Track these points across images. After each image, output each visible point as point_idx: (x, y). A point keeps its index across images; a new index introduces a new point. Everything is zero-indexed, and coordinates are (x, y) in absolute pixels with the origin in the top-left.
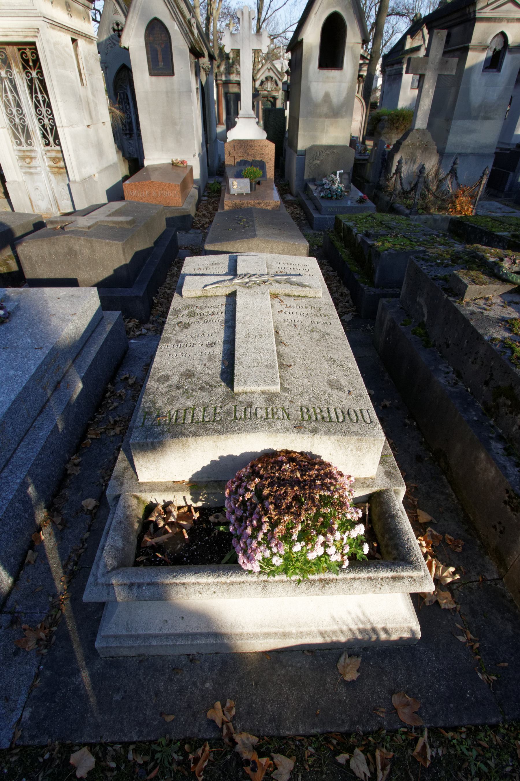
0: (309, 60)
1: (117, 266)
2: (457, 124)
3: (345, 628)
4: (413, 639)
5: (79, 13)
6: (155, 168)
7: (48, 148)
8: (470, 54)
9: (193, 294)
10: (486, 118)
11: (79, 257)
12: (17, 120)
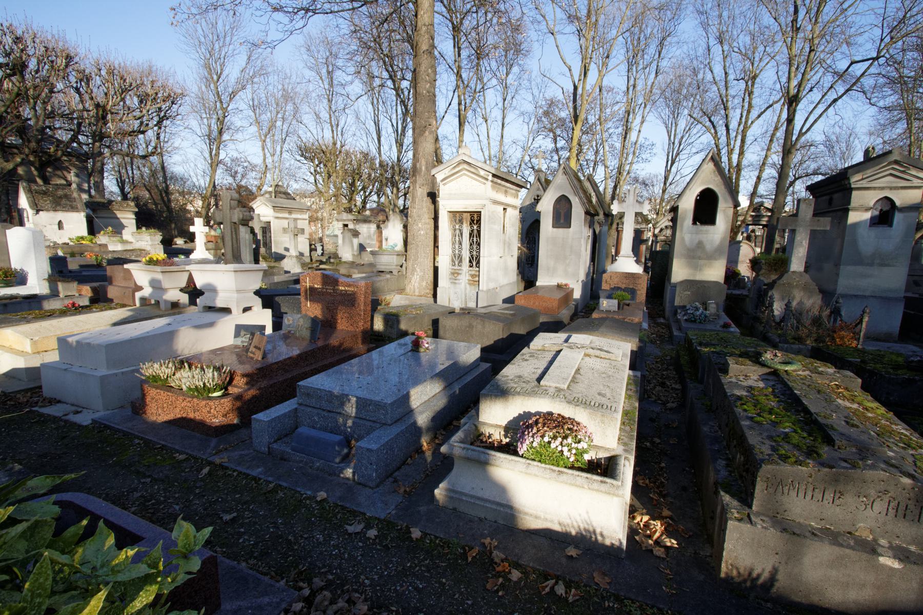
0: (684, 219)
1: (496, 338)
2: (845, 270)
3: (575, 524)
4: (619, 548)
5: (512, 195)
6: (543, 287)
10: (883, 265)
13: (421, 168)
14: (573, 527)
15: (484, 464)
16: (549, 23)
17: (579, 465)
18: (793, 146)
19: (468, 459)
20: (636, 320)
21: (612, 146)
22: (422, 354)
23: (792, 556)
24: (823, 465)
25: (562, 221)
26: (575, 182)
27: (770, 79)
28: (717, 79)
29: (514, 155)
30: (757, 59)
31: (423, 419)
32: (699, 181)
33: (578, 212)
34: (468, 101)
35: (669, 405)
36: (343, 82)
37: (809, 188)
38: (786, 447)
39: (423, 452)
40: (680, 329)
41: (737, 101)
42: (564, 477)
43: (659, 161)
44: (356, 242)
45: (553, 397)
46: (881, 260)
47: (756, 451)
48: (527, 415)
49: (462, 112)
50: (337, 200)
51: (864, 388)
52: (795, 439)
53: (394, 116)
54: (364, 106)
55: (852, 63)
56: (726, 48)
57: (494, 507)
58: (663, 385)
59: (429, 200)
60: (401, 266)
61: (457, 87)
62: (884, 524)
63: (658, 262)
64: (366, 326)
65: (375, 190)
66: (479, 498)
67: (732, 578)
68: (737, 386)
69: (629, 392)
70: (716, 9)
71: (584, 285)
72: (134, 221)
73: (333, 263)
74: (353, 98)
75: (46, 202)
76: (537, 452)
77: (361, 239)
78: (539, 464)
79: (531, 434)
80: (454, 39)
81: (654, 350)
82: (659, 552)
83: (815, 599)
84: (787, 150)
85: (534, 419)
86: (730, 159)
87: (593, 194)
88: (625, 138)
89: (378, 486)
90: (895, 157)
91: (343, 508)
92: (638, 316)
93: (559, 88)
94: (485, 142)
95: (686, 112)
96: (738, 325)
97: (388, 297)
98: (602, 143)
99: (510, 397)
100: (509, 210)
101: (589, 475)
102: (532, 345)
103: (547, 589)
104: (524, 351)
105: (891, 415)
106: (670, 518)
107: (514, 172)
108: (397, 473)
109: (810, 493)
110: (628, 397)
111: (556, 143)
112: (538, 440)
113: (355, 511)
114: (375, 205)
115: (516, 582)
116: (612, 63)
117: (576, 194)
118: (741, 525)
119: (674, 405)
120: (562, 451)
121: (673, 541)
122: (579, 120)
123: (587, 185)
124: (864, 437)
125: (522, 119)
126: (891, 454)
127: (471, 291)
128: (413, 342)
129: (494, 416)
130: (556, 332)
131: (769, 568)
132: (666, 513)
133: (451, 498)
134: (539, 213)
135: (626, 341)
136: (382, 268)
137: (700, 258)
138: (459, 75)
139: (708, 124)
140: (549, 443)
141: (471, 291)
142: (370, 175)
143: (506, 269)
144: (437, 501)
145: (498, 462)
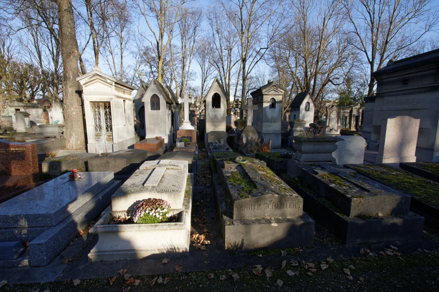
0: (208, 106)
1: (123, 167)
2: (265, 124)
4: (186, 252)
5: (128, 93)
8: (264, 104)
9: (143, 169)
10: (274, 122)
11: (110, 164)
12: (98, 123)
13: (69, 77)
14: (165, 249)
15: (117, 232)
16: (142, 9)
17: (165, 220)
18: (246, 77)
19: (106, 232)
20: (193, 150)
21: (178, 73)
22: (76, 182)
23: (247, 233)
24: (253, 196)
25: (155, 107)
26: (160, 88)
27: (236, 51)
28: (218, 48)
29: (130, 73)
30: (231, 42)
31: (78, 218)
32: (213, 90)
33: (163, 102)
34: (99, 42)
35: (207, 185)
36: (6, 18)
37: (251, 94)
38: (243, 192)
39: (81, 236)
40: (211, 152)
41: (226, 58)
42: (158, 227)
43: (196, 80)
44: (27, 120)
45: (150, 191)
46: (273, 120)
47: (233, 196)
48: (138, 202)
49: (97, 48)
50: (8, 93)
51: (268, 165)
52: (246, 189)
53: (50, 45)
54: (26, 35)
55: (261, 49)
56: (220, 36)
57: (124, 252)
58: (204, 177)
59: (77, 95)
60: (62, 133)
61: (92, 33)
62: (272, 212)
63: (201, 125)
64: (35, 171)
65: (40, 87)
66: (115, 251)
67: (230, 248)
68: (228, 172)
69: (188, 183)
70: (215, 19)
71: (169, 137)
73: (9, 134)
74: (16, 29)
76: (144, 219)
77: (31, 118)
78: (145, 224)
79: (139, 211)
80: (87, 6)
81: (201, 163)
82: (203, 248)
83: (256, 246)
84: (244, 79)
85: (141, 203)
86: (225, 81)
87: (170, 94)
88: (183, 69)
89: (49, 264)
90: (274, 84)
91: (22, 285)
92: (194, 149)
93: (151, 41)
94: (112, 65)
95: (208, 60)
96: (232, 148)
97: (54, 152)
98: (173, 71)
99: (128, 195)
100: (127, 101)
101: (169, 223)
102: (140, 168)
103: (154, 283)
104: (136, 171)
105: (274, 174)
106: (207, 232)
107: (131, 82)
108: (63, 252)
109: (251, 208)
110: (188, 185)
111: (151, 69)
112: (143, 213)
113: (32, 284)
114: (41, 97)
115: (138, 285)
116: (174, 34)
117: (161, 93)
118: (230, 226)
119: (209, 185)
120: (156, 215)
121: (209, 241)
122: (161, 58)
123: (167, 90)
124: (265, 183)
125: (132, 55)
126: (273, 187)
127: (109, 144)
128: (70, 176)
129: (121, 207)
130: (155, 160)
131: (241, 240)
132: (206, 230)
133: (99, 256)
134: (144, 103)
135: (186, 160)
136: (49, 135)
137: (216, 122)
138: (92, 26)
139: (216, 66)
140: (149, 213)
141: (109, 144)
142: (35, 79)
143: (128, 131)
144: (91, 260)
145: (123, 230)
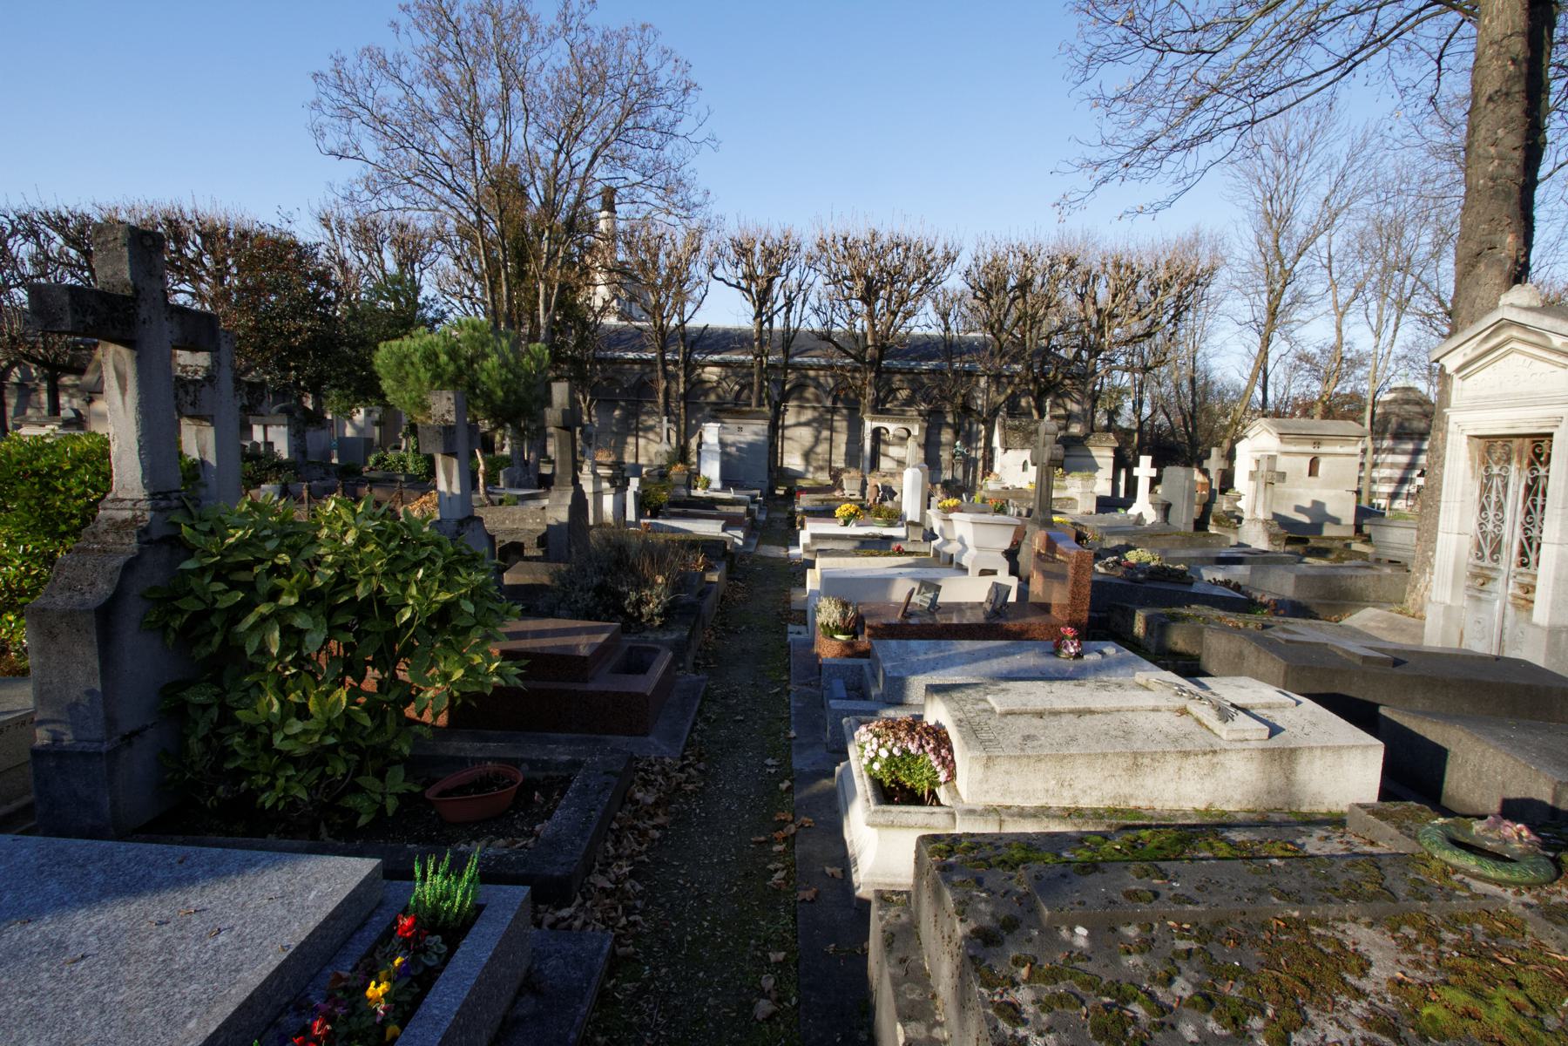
7: (1523, 569)
72: (1111, 461)
75: (1016, 439)
